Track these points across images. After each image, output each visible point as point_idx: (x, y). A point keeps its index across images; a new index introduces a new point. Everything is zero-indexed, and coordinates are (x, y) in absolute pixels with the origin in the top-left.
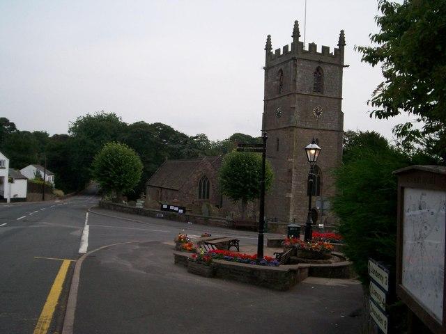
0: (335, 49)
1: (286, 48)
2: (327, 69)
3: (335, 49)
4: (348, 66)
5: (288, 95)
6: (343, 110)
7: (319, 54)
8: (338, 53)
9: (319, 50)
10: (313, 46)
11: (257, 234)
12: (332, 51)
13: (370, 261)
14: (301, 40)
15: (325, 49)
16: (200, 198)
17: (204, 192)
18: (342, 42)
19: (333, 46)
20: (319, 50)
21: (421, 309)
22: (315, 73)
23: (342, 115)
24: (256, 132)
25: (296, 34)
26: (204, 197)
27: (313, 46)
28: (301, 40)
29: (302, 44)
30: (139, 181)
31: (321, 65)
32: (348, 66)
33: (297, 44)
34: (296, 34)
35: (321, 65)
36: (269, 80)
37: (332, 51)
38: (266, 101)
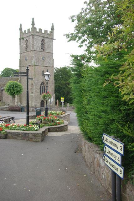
1: (29, 30)
2: (46, 40)
4: (55, 39)
5: (30, 51)
6: (53, 58)
8: (51, 33)
9: (43, 32)
15: (46, 31)
18: (53, 29)
19: (49, 30)
20: (43, 32)
22: (42, 42)
23: (53, 60)
25: (33, 24)
27: (40, 30)
32: (55, 39)
36: (22, 44)
37: (48, 32)
38: (21, 53)
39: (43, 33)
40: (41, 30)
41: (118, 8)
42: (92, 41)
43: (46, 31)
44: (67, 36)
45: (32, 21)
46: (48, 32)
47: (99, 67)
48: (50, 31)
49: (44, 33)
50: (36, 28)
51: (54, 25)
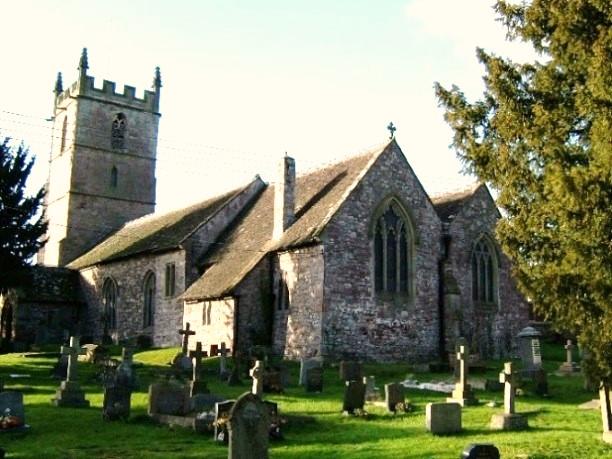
0: (147, 93)
2: (132, 118)
9: (120, 90)
14: (89, 73)
15: (130, 90)
20: (120, 90)
23: (155, 180)
25: (84, 65)
27: (109, 85)
28: (89, 73)
31: (126, 112)
34: (84, 65)
35: (126, 112)
37: (140, 95)
38: (273, 209)
39: (120, 95)
40: (113, 85)
41: (590, 429)
42: (26, 256)
43: (130, 90)
44: (392, 124)
45: (155, 76)
46: (140, 95)
47: (92, 288)
48: (146, 92)
49: (104, 91)
50: (92, 79)
51: (441, 85)
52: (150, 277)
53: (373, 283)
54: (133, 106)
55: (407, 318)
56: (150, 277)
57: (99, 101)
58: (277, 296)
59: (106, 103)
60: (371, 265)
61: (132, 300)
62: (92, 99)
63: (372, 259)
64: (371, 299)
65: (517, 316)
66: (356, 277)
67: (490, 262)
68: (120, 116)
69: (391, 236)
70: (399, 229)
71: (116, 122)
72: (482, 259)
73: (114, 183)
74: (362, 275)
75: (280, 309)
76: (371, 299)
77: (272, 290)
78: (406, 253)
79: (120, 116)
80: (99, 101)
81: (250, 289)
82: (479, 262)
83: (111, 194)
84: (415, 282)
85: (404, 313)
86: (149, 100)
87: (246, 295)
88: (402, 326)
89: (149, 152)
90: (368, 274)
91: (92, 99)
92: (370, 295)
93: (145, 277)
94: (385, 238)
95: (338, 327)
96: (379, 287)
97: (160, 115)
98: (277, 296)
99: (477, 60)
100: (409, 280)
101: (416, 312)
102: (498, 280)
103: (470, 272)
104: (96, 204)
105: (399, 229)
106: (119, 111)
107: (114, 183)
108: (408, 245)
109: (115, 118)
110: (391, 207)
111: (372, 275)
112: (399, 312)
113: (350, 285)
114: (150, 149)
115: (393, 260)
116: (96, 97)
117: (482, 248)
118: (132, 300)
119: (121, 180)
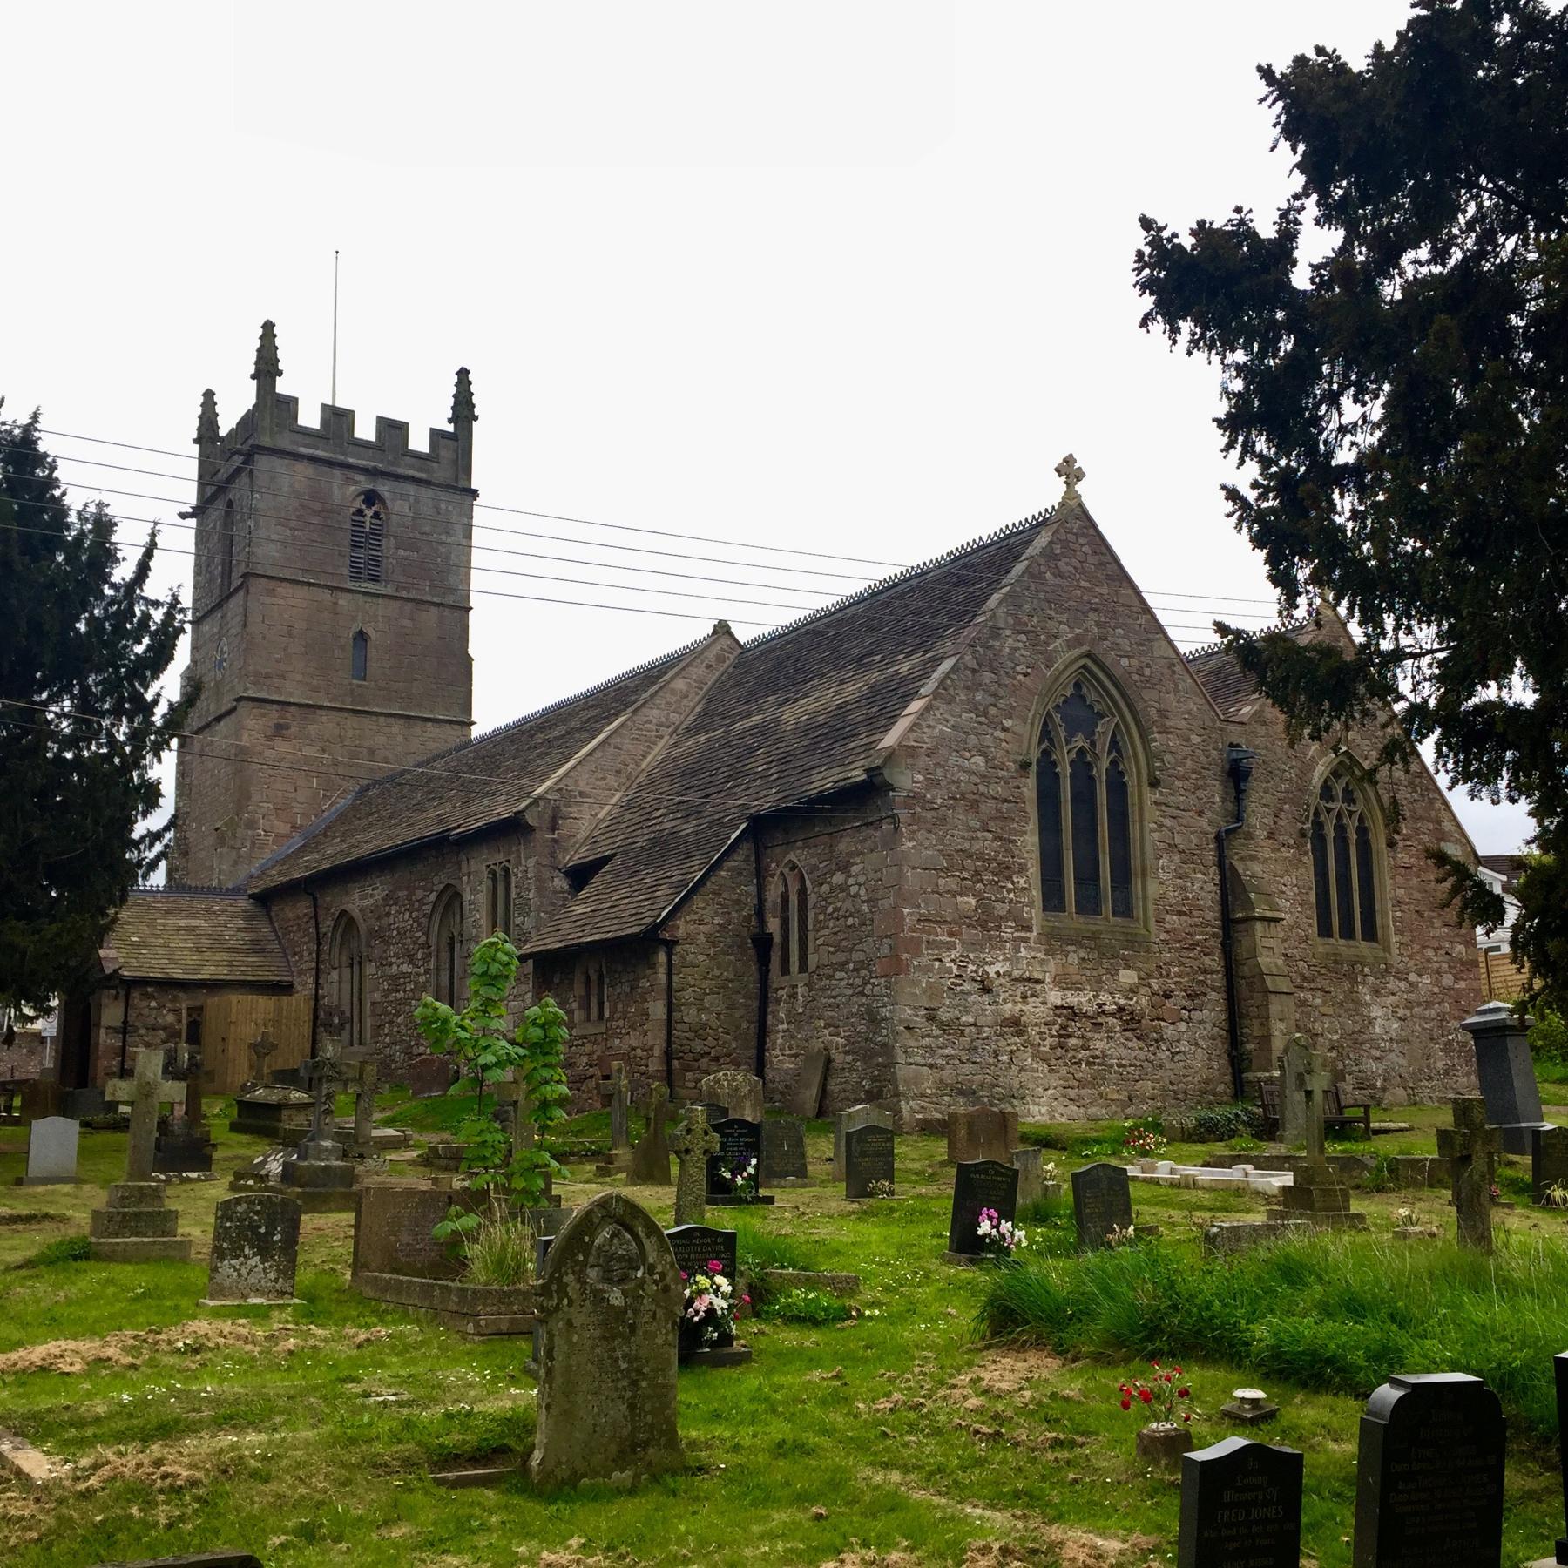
0: (436, 435)
2: (400, 503)
3: (436, 435)
7: (417, 456)
9: (365, 430)
10: (337, 418)
11: (1273, 998)
12: (419, 442)
13: (1455, 878)
14: (283, 386)
15: (392, 430)
16: (1325, 930)
17: (1085, 831)
20: (365, 430)
21: (59, 1024)
24: (1358, 62)
25: (267, 367)
26: (1090, 905)
27: (337, 418)
28: (283, 386)
29: (289, 405)
30: (1357, 633)
31: (385, 488)
33: (29, 429)
34: (267, 367)
35: (385, 488)
37: (419, 442)
52: (448, 906)
53: (1036, 893)
54: (401, 471)
55: (1133, 991)
56: (448, 906)
57: (312, 459)
58: (777, 939)
59: (330, 463)
60: (1029, 841)
61: (406, 968)
62: (297, 456)
63: (1033, 825)
64: (1033, 935)
65: (1448, 980)
66: (988, 877)
67: (1363, 831)
68: (371, 498)
69: (1082, 765)
70: (1103, 743)
71: (360, 512)
72: (1340, 829)
73: (361, 671)
74: (1005, 871)
75: (785, 970)
76: (1033, 935)
77: (762, 922)
78: (1124, 815)
79: (371, 498)
80: (312, 459)
81: (701, 922)
82: (1330, 832)
83: (201, 998)
84: (1153, 889)
85: (1128, 977)
86: (443, 453)
87: (690, 939)
88: (1121, 1009)
89: (452, 590)
90: (1022, 869)
91: (297, 456)
92: (1029, 929)
93: (435, 904)
94: (1065, 770)
95: (943, 1015)
96: (1053, 898)
97: (474, 494)
98: (777, 939)
99: (1126, 275)
100: (1137, 884)
101: (1161, 971)
102: (1389, 882)
103: (1308, 860)
104: (313, 729)
105: (1103, 743)
106: (365, 483)
107: (361, 671)
108: (1132, 790)
109: (359, 503)
110: (1077, 686)
111: (1034, 870)
112: (1113, 973)
113: (973, 901)
114: (452, 580)
115: (1085, 831)
116: (303, 450)
117: (1339, 790)
118: (406, 968)
119: (377, 665)
